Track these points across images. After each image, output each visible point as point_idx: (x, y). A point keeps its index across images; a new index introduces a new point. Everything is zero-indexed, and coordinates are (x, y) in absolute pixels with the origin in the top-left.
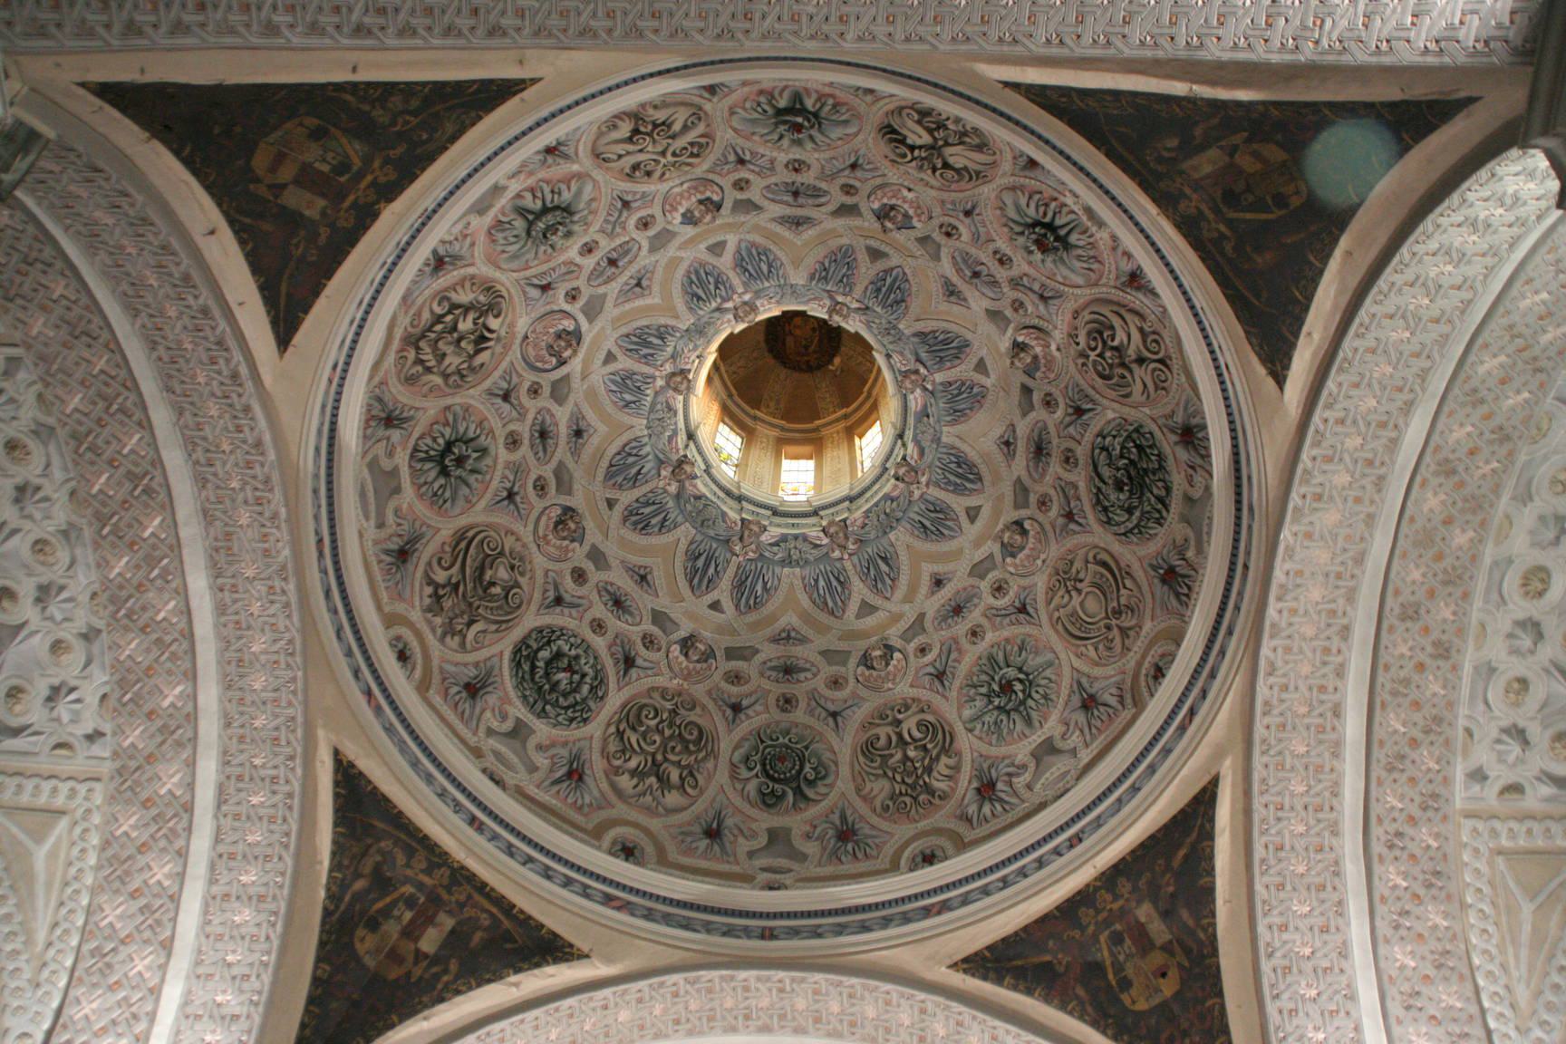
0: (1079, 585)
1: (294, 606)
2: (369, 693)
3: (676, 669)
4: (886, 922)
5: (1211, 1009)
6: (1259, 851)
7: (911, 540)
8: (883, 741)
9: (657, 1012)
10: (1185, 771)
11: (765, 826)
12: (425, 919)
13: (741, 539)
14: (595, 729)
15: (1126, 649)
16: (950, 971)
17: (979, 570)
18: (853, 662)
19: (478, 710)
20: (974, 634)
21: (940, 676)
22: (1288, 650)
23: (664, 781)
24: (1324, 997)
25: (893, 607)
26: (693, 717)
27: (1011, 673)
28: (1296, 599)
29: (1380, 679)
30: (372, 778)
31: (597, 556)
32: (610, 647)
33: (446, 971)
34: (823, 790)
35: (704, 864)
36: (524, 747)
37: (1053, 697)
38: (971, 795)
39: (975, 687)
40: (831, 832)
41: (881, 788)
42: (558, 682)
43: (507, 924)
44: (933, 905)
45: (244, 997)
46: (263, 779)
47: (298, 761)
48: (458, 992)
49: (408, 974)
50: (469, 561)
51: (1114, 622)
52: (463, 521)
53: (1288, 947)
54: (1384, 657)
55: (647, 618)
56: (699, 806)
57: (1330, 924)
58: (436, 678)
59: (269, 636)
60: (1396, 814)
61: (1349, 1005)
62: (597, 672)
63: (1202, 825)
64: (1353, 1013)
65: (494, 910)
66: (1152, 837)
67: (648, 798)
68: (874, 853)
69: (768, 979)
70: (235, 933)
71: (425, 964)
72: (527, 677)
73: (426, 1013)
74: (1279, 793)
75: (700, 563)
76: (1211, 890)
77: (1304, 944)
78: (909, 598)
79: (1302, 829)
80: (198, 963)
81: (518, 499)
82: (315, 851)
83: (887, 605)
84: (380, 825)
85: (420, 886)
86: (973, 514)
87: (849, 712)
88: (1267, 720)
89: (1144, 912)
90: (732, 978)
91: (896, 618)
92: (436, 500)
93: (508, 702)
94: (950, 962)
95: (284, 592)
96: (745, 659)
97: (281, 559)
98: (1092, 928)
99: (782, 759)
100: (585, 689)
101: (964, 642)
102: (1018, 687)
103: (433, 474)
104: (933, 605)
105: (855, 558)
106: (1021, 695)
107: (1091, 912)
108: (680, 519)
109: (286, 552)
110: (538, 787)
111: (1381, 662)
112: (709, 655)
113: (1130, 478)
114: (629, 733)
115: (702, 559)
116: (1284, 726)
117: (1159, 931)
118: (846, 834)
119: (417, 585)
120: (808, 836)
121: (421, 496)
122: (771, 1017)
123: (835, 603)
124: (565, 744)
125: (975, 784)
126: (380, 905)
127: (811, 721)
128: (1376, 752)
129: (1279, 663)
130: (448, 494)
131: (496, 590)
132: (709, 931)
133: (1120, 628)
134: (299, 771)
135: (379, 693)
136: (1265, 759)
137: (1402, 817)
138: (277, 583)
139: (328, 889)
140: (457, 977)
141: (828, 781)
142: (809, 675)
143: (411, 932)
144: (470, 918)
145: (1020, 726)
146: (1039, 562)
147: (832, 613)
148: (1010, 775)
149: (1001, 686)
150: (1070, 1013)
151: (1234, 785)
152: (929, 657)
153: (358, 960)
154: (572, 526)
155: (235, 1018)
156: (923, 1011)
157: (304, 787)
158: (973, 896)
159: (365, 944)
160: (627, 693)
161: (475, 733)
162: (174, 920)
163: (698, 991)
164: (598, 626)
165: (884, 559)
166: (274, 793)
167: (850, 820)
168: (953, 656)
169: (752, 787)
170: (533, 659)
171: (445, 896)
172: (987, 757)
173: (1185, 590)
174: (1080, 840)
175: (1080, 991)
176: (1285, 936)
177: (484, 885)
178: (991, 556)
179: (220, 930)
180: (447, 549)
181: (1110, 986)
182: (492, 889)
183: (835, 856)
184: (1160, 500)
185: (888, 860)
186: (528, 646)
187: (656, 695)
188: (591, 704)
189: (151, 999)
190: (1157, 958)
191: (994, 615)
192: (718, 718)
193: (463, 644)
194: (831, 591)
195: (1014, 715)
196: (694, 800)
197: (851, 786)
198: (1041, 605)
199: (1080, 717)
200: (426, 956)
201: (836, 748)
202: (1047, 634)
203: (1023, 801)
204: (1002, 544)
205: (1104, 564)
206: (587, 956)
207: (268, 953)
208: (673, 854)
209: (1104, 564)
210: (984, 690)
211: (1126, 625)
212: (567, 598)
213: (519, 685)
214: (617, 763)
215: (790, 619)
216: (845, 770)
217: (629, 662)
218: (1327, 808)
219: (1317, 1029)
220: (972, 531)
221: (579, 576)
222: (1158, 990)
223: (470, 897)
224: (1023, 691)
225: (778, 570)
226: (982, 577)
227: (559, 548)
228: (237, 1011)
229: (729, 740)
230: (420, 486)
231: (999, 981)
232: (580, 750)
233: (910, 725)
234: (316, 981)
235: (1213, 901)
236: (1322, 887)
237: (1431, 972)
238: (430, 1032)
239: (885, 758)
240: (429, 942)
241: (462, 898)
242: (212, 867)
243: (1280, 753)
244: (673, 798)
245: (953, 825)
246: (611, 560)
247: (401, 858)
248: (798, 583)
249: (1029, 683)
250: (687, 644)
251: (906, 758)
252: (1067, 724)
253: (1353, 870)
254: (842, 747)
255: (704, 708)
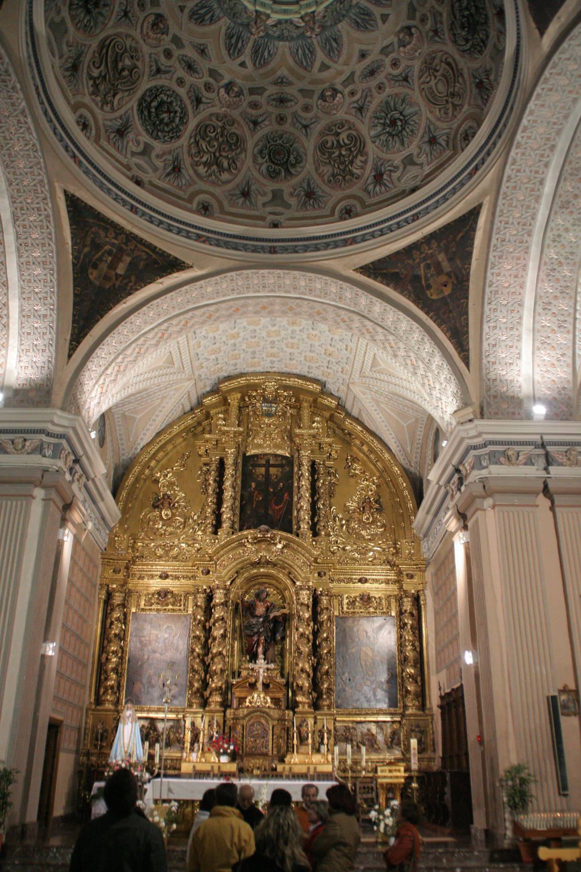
0: (435, 73)
1: (32, 128)
2: (74, 157)
3: (223, 102)
4: (327, 246)
5: (463, 303)
6: (494, 241)
7: (349, 29)
8: (329, 144)
9: (224, 287)
10: (468, 198)
11: (271, 188)
12: (117, 259)
13: (256, 23)
14: (184, 141)
15: (454, 117)
16: (354, 272)
17: (385, 51)
18: (316, 96)
19: (125, 142)
20: (380, 88)
21: (360, 109)
22: (523, 154)
23: (220, 166)
24: (510, 304)
25: (340, 68)
26: (233, 129)
27: (397, 116)
28: (531, 132)
29: (566, 168)
30: (83, 199)
31: (177, 41)
32: (188, 94)
33: (130, 281)
34: (300, 170)
35: (241, 211)
36: (150, 158)
37: (416, 132)
38: (371, 180)
39: (378, 119)
40: (303, 193)
41: (327, 170)
42: (163, 119)
43: (154, 256)
44: (349, 239)
45: (46, 307)
46: (33, 209)
47: (49, 200)
48: (137, 290)
49: (114, 285)
50: (109, 59)
51: (450, 100)
52: (102, 36)
53: (499, 282)
54: (570, 158)
55: (206, 74)
56: (238, 179)
57: (519, 276)
58: (103, 130)
59: (22, 143)
60: (559, 227)
61: (520, 308)
62: (182, 109)
63: (471, 225)
64: (521, 312)
65: (147, 250)
66: (449, 224)
67: (213, 177)
68: (323, 206)
69: (273, 273)
70: (36, 279)
71: (121, 279)
72: (147, 118)
73: (124, 300)
74: (508, 217)
75: (233, 41)
76: (471, 253)
77: (506, 282)
78: (346, 64)
79: (515, 232)
80: (23, 293)
81: (130, 15)
82: (63, 238)
83: (335, 66)
84: (91, 221)
85: (113, 245)
86: (385, 18)
87: (312, 126)
88: (508, 184)
89: (441, 257)
90: (257, 273)
91: (340, 73)
92: (86, 29)
93: (140, 134)
94: (354, 268)
95: (26, 123)
96: (259, 94)
97: (21, 107)
98: (418, 260)
99: (279, 153)
100: (177, 120)
101: (374, 91)
102: (399, 123)
103: (82, 15)
104: (360, 68)
105: (319, 37)
106: (400, 128)
107: (418, 253)
108: (221, 15)
109: (24, 103)
110: (159, 179)
111: (568, 160)
112: (240, 94)
113: (469, 24)
114: (201, 142)
115: (235, 38)
116: (515, 187)
117: (446, 266)
118: (310, 194)
119: (84, 80)
120: (291, 194)
121: (78, 29)
122: (275, 287)
123: (307, 63)
124: (170, 152)
125: (373, 174)
126: (97, 256)
127: (292, 130)
128: (557, 200)
129: (518, 160)
130: (92, 24)
131: (126, 73)
132: (246, 250)
133: (452, 103)
134: (50, 205)
135: (78, 155)
136: (504, 201)
137: (562, 228)
138: (22, 118)
139: (73, 255)
140: (135, 284)
141: (302, 165)
142: (293, 103)
143: (112, 266)
144: (138, 256)
145: (398, 145)
146: (417, 54)
147: (305, 68)
148: (390, 171)
149: (391, 121)
150: (404, 296)
151: (488, 210)
152: (356, 98)
153: (91, 283)
154: (162, 26)
155: (45, 316)
156: (342, 288)
157: (53, 211)
158: (367, 237)
159: (93, 275)
160: (199, 118)
161: (126, 157)
162: (6, 273)
163: (242, 278)
164: (181, 82)
165: (335, 40)
166: (40, 215)
167: (312, 186)
168: (368, 99)
169: (264, 168)
170: (149, 107)
171: (125, 248)
172: (380, 159)
173: (486, 97)
174: (418, 218)
175: (410, 287)
176: (499, 278)
177: (142, 240)
178: (392, 44)
179: (28, 278)
180: (97, 55)
181: (423, 286)
182: (146, 241)
183: (304, 206)
184: (483, 41)
185: (329, 210)
186: (146, 101)
187: (214, 118)
188: (181, 128)
189: (5, 297)
190: (444, 278)
191: (393, 78)
192: (246, 129)
193: (112, 108)
194: (305, 58)
195: (396, 138)
196: (236, 176)
197: (313, 167)
198: (416, 78)
199: (426, 148)
200: (120, 276)
201: (306, 145)
202: (417, 96)
203: (395, 187)
204: (399, 39)
205: (449, 64)
206: (192, 267)
207: (53, 287)
208: (227, 208)
209: (449, 64)
210: (382, 121)
211: (456, 103)
212: (163, 68)
213: (144, 123)
214: (196, 159)
215: (283, 72)
216: (310, 159)
217: (198, 101)
218: (528, 224)
219: (503, 317)
220: (383, 28)
221: (168, 54)
222: (442, 292)
223: (136, 246)
224: (401, 126)
225: (276, 43)
226: (387, 55)
227: (156, 39)
228: (45, 312)
229: (252, 142)
230: (77, 24)
231: (375, 279)
232: (178, 154)
233: (343, 136)
234: (75, 295)
235: (471, 258)
236: (518, 258)
237: (558, 295)
238: (127, 307)
239: (331, 154)
240: (121, 269)
241: (133, 247)
242: (18, 250)
243: (512, 199)
244: (225, 176)
245: (361, 194)
246: (184, 42)
247: (102, 234)
248: (287, 50)
249: (405, 123)
250: (229, 87)
251: (340, 155)
252: (421, 149)
253: (534, 251)
254: (309, 145)
255: (239, 124)
